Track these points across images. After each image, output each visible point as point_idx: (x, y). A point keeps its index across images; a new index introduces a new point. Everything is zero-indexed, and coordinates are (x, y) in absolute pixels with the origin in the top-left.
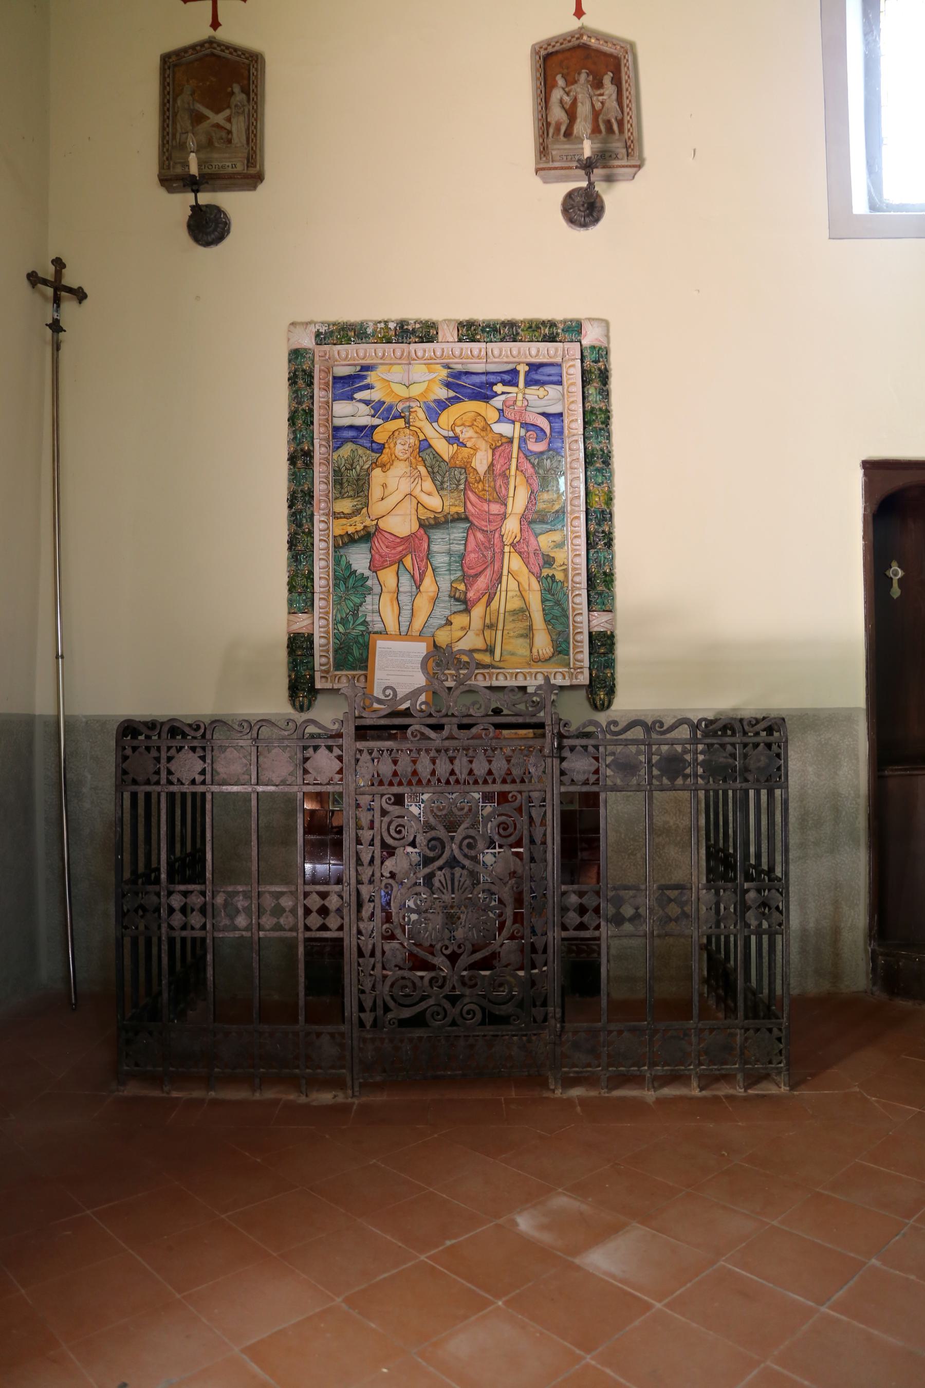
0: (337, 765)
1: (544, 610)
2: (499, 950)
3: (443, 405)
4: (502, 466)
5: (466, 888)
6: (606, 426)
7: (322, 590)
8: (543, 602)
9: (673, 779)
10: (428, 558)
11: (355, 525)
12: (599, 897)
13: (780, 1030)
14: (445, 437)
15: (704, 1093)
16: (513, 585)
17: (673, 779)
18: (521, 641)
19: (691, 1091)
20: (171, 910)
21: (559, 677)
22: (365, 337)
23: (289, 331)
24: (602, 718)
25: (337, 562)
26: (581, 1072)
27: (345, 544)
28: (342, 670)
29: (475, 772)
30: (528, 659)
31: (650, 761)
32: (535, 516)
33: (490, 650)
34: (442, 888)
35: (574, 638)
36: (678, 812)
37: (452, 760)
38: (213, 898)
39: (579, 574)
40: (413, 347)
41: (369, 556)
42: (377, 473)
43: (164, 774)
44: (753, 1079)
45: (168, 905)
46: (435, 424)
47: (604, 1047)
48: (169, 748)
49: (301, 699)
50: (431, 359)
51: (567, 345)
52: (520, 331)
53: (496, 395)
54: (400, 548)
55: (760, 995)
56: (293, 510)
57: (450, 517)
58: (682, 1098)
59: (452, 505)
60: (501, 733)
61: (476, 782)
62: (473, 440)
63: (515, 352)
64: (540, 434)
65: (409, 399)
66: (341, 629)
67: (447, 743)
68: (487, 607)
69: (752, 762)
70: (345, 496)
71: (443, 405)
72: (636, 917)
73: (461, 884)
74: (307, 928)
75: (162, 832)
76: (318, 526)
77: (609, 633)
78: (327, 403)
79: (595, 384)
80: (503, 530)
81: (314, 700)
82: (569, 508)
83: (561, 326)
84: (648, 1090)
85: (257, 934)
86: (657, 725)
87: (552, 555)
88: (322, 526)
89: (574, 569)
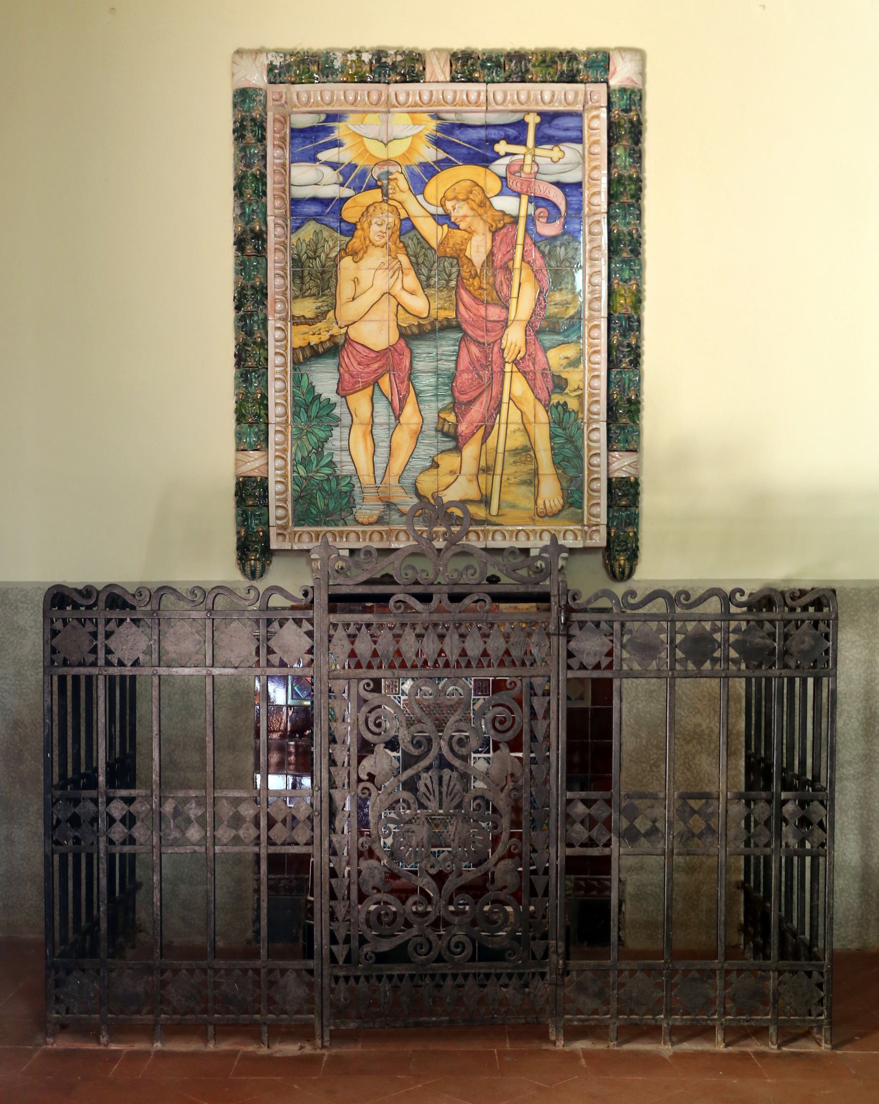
0: (306, 642)
1: (552, 449)
2: (493, 869)
3: (430, 170)
4: (504, 255)
5: (456, 794)
6: (637, 201)
7: (278, 419)
8: (551, 438)
9: (699, 663)
10: (410, 379)
11: (319, 334)
12: (610, 806)
13: (822, 974)
14: (433, 215)
15: (730, 1049)
16: (515, 416)
17: (699, 663)
18: (524, 489)
19: (715, 1046)
20: (111, 821)
21: (570, 536)
22: (332, 74)
23: (233, 62)
24: (619, 589)
25: (297, 383)
26: (587, 1020)
27: (307, 360)
28: (303, 525)
29: (469, 652)
30: (532, 513)
31: (673, 640)
32: (544, 323)
33: (486, 501)
34: (428, 794)
35: (589, 487)
36: (712, 712)
37: (442, 637)
38: (160, 806)
39: (597, 402)
40: (393, 87)
41: (337, 376)
42: (347, 262)
43: (101, 653)
44: (788, 1036)
45: (108, 814)
46: (420, 197)
47: (614, 989)
48: (108, 621)
49: (253, 562)
50: (416, 105)
51: (590, 87)
52: (530, 66)
53: (498, 157)
54: (376, 366)
55: (802, 937)
56: (241, 313)
57: (438, 325)
58: (703, 1053)
59: (441, 308)
60: (498, 607)
61: (468, 665)
62: (468, 219)
63: (523, 97)
64: (554, 212)
65: (388, 161)
66: (302, 472)
67: (435, 617)
68: (482, 444)
69: (794, 644)
70: (307, 294)
71: (430, 170)
72: (653, 832)
73: (450, 788)
74: (271, 842)
75: (100, 724)
76: (273, 335)
77: (632, 479)
78: (283, 165)
79: (624, 143)
80: (504, 342)
81: (269, 565)
82: (587, 313)
83: (583, 60)
84: (665, 1044)
85: (212, 850)
86: (682, 597)
87: (564, 375)
88: (279, 334)
89: (591, 395)
